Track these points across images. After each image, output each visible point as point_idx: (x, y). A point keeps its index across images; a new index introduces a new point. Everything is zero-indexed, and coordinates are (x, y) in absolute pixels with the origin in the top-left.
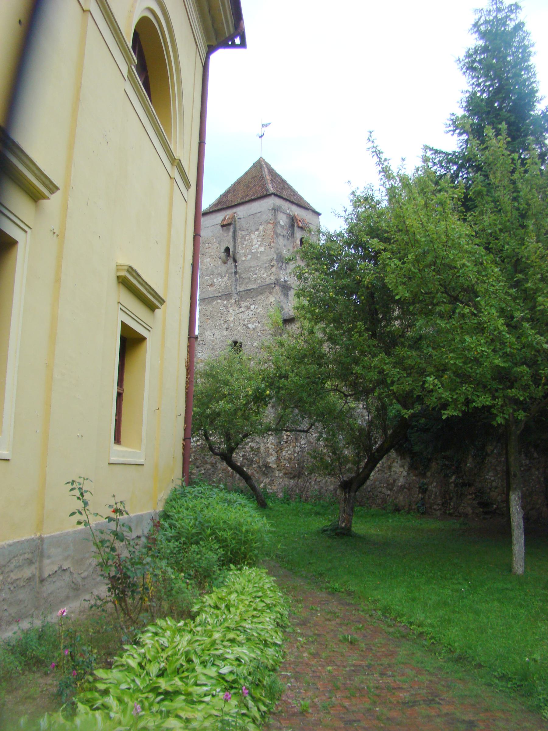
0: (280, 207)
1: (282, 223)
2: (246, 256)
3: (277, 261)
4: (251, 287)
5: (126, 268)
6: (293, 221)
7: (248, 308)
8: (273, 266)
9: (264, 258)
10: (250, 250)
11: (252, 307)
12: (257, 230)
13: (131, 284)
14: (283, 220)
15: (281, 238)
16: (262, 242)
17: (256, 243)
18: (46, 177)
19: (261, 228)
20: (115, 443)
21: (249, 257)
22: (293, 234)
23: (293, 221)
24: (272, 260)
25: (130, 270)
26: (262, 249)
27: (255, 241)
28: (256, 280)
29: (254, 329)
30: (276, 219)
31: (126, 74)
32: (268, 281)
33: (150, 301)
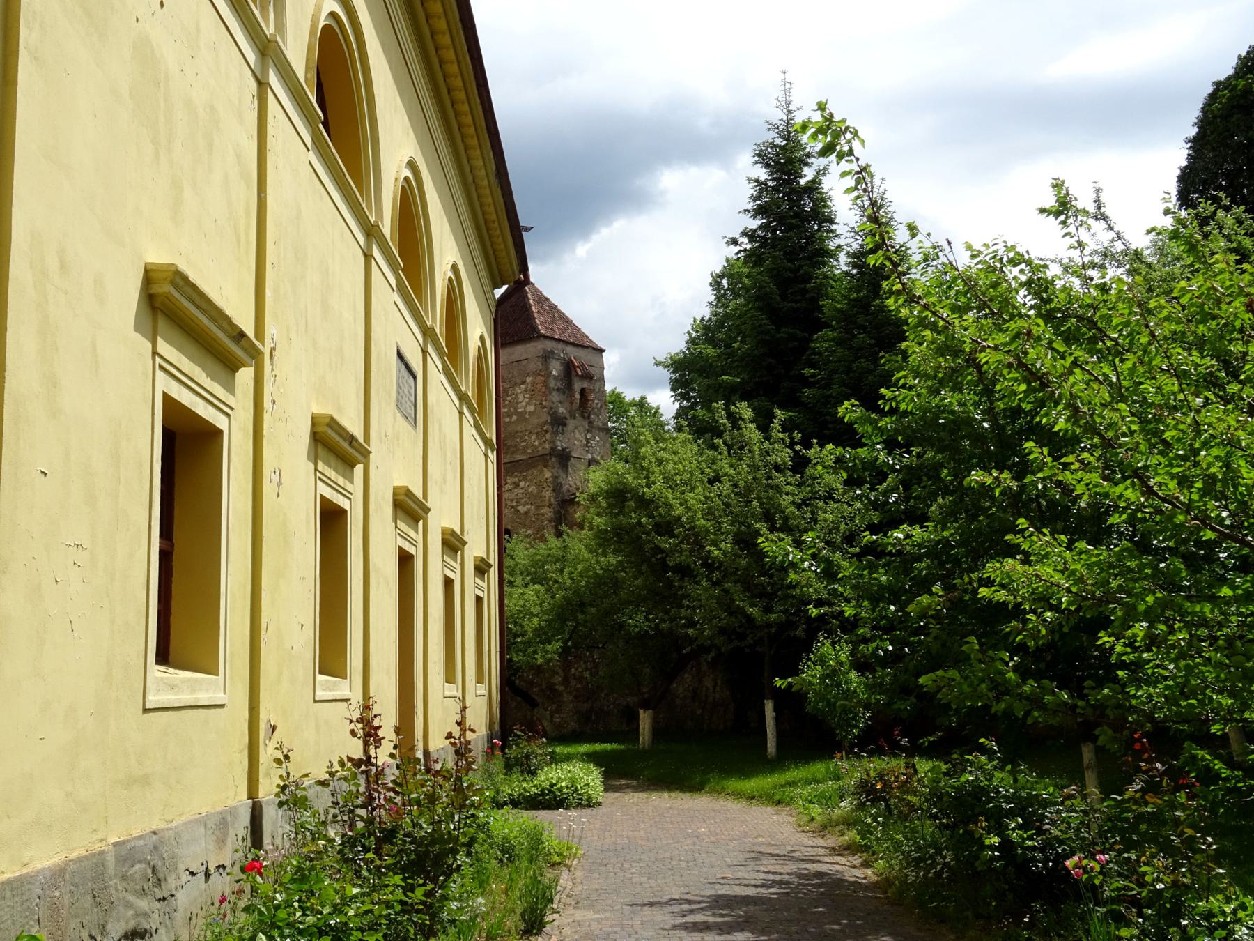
0: (552, 352)
1: (554, 373)
2: (510, 416)
3: (552, 424)
4: (519, 457)
5: (327, 420)
6: (569, 367)
7: (517, 485)
8: (546, 432)
9: (535, 421)
10: (515, 409)
11: (522, 484)
12: (523, 383)
13: (170, 305)
14: (556, 369)
15: (554, 393)
16: (530, 399)
17: (523, 399)
18: (194, 287)
19: (529, 380)
20: (157, 662)
21: (514, 418)
22: (569, 387)
23: (569, 367)
24: (545, 423)
25: (178, 280)
26: (531, 408)
27: (521, 397)
28: (525, 448)
29: (526, 513)
30: (547, 368)
31: (440, 367)
32: (541, 451)
33: (222, 346)
